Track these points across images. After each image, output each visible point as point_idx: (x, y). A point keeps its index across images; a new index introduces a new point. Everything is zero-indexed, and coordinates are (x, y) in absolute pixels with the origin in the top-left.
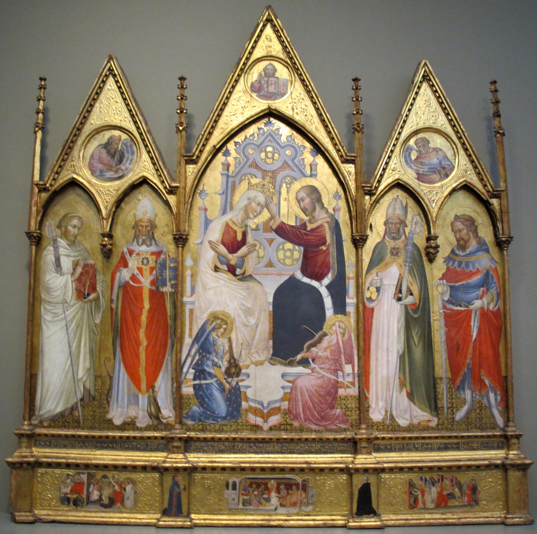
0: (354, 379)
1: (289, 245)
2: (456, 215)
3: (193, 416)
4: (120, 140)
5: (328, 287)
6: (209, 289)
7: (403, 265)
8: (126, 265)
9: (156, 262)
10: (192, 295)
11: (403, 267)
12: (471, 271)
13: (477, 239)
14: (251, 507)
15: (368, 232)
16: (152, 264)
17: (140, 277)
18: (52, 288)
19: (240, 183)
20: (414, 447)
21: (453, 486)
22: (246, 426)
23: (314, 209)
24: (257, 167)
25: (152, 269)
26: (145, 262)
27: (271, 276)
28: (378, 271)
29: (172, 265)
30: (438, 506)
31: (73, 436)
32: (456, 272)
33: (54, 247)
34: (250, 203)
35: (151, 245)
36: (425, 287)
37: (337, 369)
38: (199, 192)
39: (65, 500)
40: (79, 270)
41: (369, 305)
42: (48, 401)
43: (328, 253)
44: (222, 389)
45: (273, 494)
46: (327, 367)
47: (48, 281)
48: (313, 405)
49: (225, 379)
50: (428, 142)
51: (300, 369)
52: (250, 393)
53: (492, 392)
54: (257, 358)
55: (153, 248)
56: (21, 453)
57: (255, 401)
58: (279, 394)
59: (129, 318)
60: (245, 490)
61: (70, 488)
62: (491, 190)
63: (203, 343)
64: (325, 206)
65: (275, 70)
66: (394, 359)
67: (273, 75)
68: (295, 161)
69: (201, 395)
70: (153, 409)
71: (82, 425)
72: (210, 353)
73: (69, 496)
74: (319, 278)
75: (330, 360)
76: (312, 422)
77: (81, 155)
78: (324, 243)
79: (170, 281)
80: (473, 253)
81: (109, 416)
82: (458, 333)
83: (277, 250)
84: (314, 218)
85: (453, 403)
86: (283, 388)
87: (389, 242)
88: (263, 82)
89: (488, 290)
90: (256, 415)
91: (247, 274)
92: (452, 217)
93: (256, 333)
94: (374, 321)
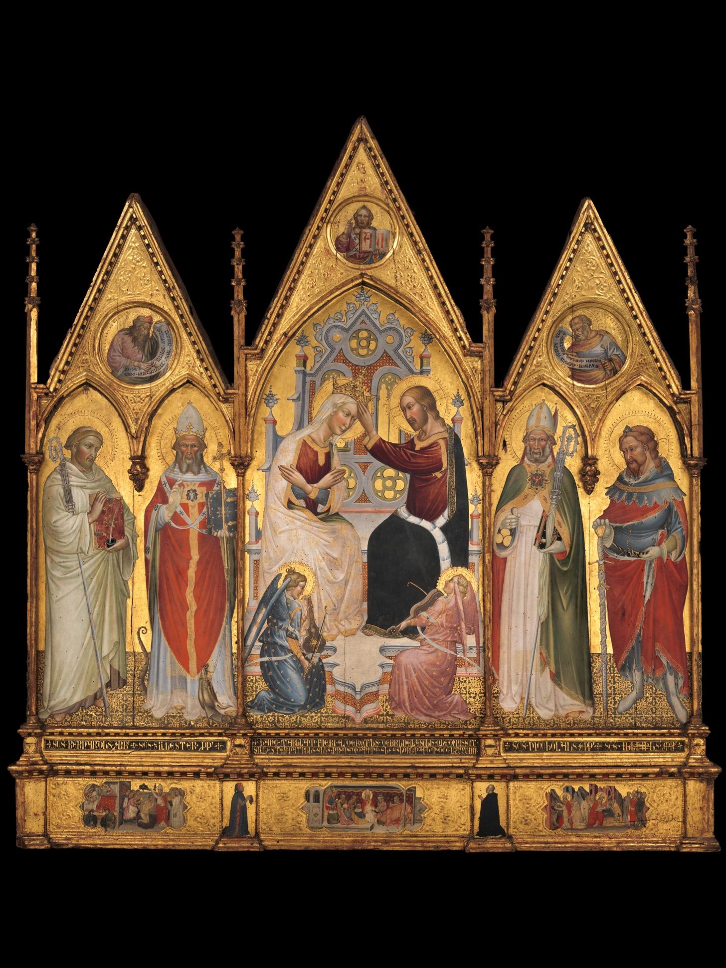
0: (478, 654)
1: (390, 472)
2: (627, 427)
3: (260, 705)
4: (151, 323)
5: (444, 529)
6: (280, 533)
7: (548, 499)
8: (165, 501)
9: (207, 495)
10: (257, 542)
11: (549, 501)
12: (645, 506)
13: (657, 461)
14: (339, 825)
15: (501, 453)
16: (201, 498)
17: (184, 516)
18: (62, 533)
19: (321, 384)
20: (559, 747)
21: (611, 799)
22: (333, 717)
23: (425, 421)
24: (346, 361)
25: (201, 506)
26: (192, 495)
27: (366, 515)
28: (513, 506)
29: (229, 500)
30: (590, 826)
32: (624, 507)
33: (61, 475)
34: (336, 413)
35: (199, 473)
36: (579, 528)
37: (456, 641)
38: (265, 397)
40: (99, 507)
41: (502, 554)
42: (61, 688)
43: (445, 482)
44: (300, 669)
45: (369, 808)
46: (442, 638)
47: (55, 522)
48: (422, 689)
49: (304, 654)
50: (590, 323)
51: (405, 641)
52: (337, 673)
53: (671, 674)
54: (347, 626)
55: (202, 477)
57: (344, 684)
58: (377, 675)
59: (171, 574)
60: (331, 802)
61: (96, 803)
62: (677, 393)
63: (273, 607)
64: (441, 415)
65: (370, 216)
66: (533, 627)
67: (368, 225)
68: (399, 351)
69: (271, 677)
70: (206, 697)
72: (283, 620)
74: (432, 517)
75: (446, 629)
76: (421, 711)
77: (97, 345)
78: (439, 468)
79: (227, 522)
80: (650, 481)
82: (624, 592)
83: (374, 478)
84: (425, 432)
85: (615, 689)
86: (382, 666)
87: (529, 466)
88: (353, 236)
89: (669, 532)
90: (345, 703)
91: (332, 512)
92: (620, 430)
93: (345, 591)
94: (507, 576)
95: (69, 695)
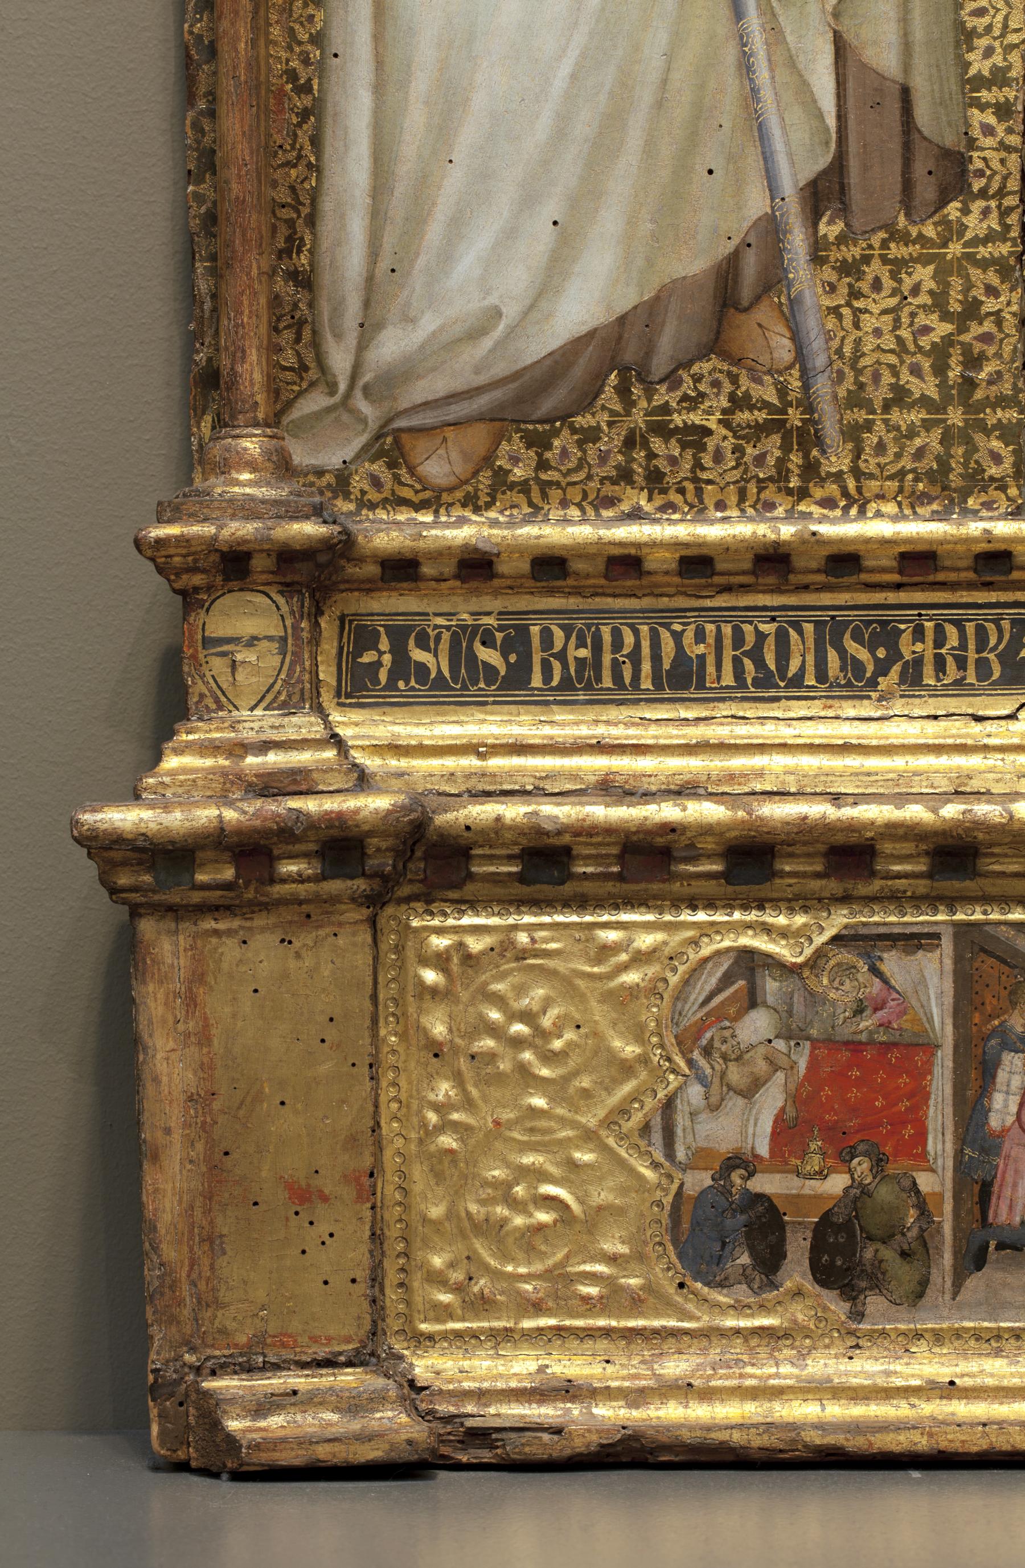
31: (772, 562)
39: (731, 1235)
56: (244, 748)
61: (772, 1100)
73: (765, 1184)
95: (514, 284)
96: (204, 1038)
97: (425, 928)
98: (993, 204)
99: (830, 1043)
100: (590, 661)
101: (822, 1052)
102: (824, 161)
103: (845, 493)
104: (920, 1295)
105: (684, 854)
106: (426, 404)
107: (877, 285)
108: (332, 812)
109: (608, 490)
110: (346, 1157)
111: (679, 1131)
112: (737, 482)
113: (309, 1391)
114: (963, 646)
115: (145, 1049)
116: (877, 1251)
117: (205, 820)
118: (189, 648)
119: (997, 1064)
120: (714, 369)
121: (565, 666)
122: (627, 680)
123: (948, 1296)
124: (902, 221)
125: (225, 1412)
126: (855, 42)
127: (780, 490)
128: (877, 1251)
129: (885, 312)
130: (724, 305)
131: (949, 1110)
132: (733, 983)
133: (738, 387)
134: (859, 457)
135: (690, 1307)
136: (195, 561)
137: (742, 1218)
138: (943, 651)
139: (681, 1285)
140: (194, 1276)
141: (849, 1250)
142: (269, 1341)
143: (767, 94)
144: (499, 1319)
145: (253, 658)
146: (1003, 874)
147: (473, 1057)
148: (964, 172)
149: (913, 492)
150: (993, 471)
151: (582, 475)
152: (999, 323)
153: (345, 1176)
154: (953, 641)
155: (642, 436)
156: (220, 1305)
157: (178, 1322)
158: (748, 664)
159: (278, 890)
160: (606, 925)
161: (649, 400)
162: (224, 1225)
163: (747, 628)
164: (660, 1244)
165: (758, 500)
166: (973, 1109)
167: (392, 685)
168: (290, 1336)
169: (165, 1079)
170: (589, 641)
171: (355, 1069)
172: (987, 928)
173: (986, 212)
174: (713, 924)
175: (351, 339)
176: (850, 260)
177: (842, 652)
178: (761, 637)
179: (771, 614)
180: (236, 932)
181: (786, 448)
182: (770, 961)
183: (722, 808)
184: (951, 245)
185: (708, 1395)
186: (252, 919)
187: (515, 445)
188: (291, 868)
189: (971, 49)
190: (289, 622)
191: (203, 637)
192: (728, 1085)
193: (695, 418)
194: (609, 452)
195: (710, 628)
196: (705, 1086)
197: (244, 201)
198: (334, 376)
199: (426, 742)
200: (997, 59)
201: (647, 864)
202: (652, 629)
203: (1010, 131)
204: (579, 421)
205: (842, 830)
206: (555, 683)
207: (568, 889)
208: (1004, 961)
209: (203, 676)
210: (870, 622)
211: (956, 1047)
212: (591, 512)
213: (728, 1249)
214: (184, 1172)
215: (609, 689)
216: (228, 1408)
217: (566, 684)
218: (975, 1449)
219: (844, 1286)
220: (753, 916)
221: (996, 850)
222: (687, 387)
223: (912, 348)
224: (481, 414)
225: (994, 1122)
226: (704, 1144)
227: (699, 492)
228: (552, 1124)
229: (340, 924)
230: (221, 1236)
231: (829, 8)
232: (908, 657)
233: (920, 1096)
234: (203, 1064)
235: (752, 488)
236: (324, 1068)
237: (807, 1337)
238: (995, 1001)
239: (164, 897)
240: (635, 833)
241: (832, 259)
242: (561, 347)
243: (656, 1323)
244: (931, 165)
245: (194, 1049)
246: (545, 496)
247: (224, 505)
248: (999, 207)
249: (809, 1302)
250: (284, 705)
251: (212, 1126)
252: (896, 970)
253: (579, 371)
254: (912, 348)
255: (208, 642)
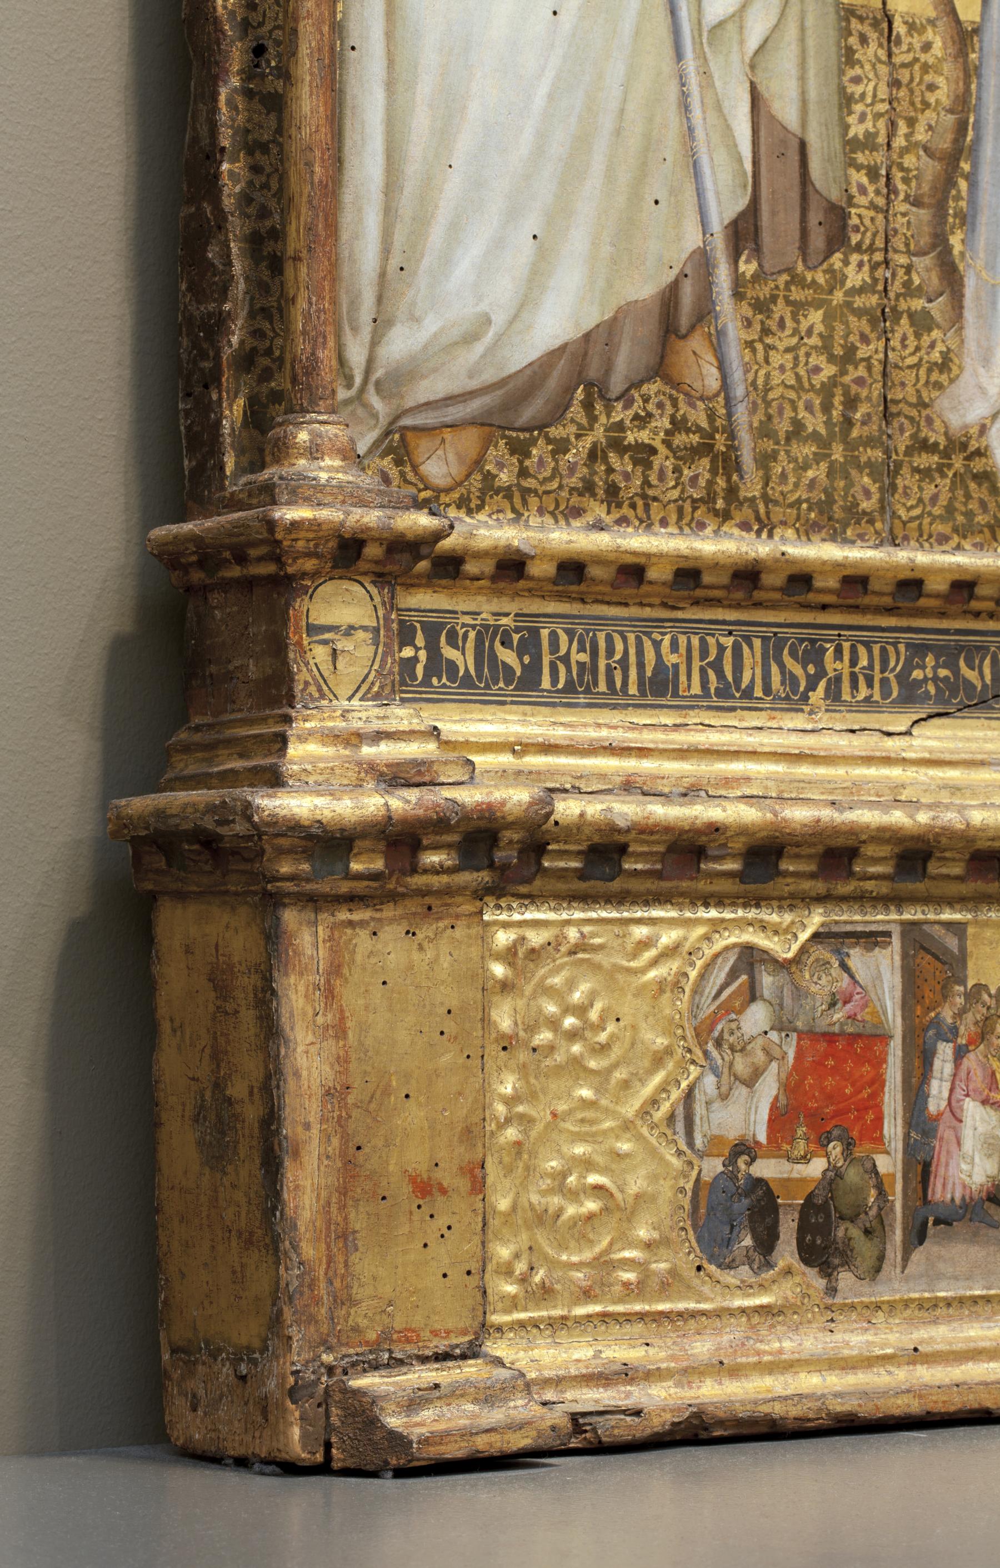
31: (747, 576)
42: (455, 229)
61: (769, 1088)
71: (751, 487)
73: (766, 1169)
81: (963, 408)
95: (501, 293)
96: (340, 1031)
97: (495, 923)
98: (866, 258)
99: (810, 1035)
100: (588, 665)
101: (806, 1043)
102: (742, 203)
103: (758, 519)
104: (878, 1270)
105: (716, 853)
106: (428, 404)
107: (782, 324)
108: (483, 803)
109: (575, 500)
110: (462, 1149)
111: (697, 1120)
112: (676, 501)
113: (450, 1384)
114: (871, 667)
115: (287, 1042)
116: (847, 1229)
117: (372, 808)
118: (295, 633)
119: (933, 1053)
120: (659, 391)
121: (569, 670)
122: (618, 685)
123: (898, 1270)
124: (800, 267)
125: (382, 1409)
126: (766, 95)
127: (709, 510)
128: (847, 1229)
129: (788, 350)
130: (667, 331)
131: (899, 1096)
132: (738, 977)
133: (678, 410)
134: (767, 485)
135: (706, 1289)
136: (316, 546)
137: (746, 1202)
138: (857, 670)
139: (699, 1268)
140: (331, 1273)
141: (826, 1229)
142: (395, 1336)
143: (700, 133)
144: (555, 1307)
145: (350, 647)
146: (948, 877)
147: (534, 1050)
148: (844, 226)
149: (807, 520)
150: (865, 505)
151: (555, 485)
152: (869, 368)
153: (461, 1168)
154: (864, 662)
155: (603, 451)
156: (353, 1302)
157: (317, 1322)
158: (712, 675)
159: (418, 881)
160: (639, 921)
161: (608, 416)
162: (358, 1221)
163: (711, 641)
164: (683, 1229)
165: (693, 519)
166: (917, 1095)
167: (426, 682)
168: (414, 1331)
169: (304, 1073)
170: (588, 645)
171: (470, 1061)
172: (925, 927)
173: (860, 265)
174: (723, 920)
175: (366, 331)
176: (762, 298)
177: (782, 666)
178: (721, 649)
179: (729, 628)
180: (368, 923)
181: (714, 471)
182: (766, 957)
183: (753, 810)
184: (835, 292)
185: (735, 1372)
186: (381, 910)
187: (499, 451)
188: (433, 858)
189: (850, 113)
190: (381, 613)
191: (307, 623)
192: (735, 1075)
193: (644, 436)
194: (576, 463)
195: (682, 640)
196: (717, 1076)
197: (327, 185)
198: (351, 369)
199: (472, 739)
200: (869, 124)
201: (683, 862)
202: (638, 638)
203: (877, 192)
204: (554, 432)
205: (845, 833)
206: (560, 686)
207: (616, 885)
208: (937, 958)
209: (307, 664)
210: (803, 640)
211: (904, 1038)
212: (562, 522)
213: (735, 1232)
214: (322, 1168)
215: (604, 693)
216: (383, 1404)
217: (570, 688)
218: (952, 1409)
219: (823, 1263)
220: (752, 914)
221: (948, 854)
222: (637, 407)
223: (806, 385)
224: (474, 418)
225: (933, 1107)
226: (716, 1132)
227: (647, 507)
228: (599, 1114)
229: (457, 917)
230: (355, 1232)
231: (747, 60)
232: (831, 674)
233: (878, 1082)
234: (339, 1057)
235: (688, 507)
236: (446, 1059)
237: (795, 1313)
238: (931, 995)
239: (316, 886)
240: (687, 832)
241: (749, 295)
242: (539, 359)
243: (681, 1306)
244: (821, 217)
245: (331, 1042)
246: (525, 503)
247: (335, 491)
248: (869, 261)
249: (798, 1279)
250: (377, 696)
251: (347, 1120)
252: (859, 965)
253: (553, 383)
254: (806, 385)
255: (313, 629)
